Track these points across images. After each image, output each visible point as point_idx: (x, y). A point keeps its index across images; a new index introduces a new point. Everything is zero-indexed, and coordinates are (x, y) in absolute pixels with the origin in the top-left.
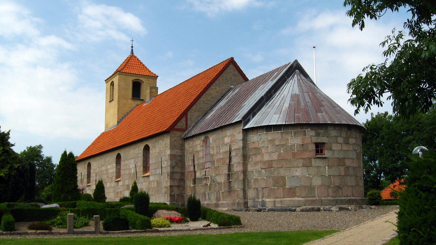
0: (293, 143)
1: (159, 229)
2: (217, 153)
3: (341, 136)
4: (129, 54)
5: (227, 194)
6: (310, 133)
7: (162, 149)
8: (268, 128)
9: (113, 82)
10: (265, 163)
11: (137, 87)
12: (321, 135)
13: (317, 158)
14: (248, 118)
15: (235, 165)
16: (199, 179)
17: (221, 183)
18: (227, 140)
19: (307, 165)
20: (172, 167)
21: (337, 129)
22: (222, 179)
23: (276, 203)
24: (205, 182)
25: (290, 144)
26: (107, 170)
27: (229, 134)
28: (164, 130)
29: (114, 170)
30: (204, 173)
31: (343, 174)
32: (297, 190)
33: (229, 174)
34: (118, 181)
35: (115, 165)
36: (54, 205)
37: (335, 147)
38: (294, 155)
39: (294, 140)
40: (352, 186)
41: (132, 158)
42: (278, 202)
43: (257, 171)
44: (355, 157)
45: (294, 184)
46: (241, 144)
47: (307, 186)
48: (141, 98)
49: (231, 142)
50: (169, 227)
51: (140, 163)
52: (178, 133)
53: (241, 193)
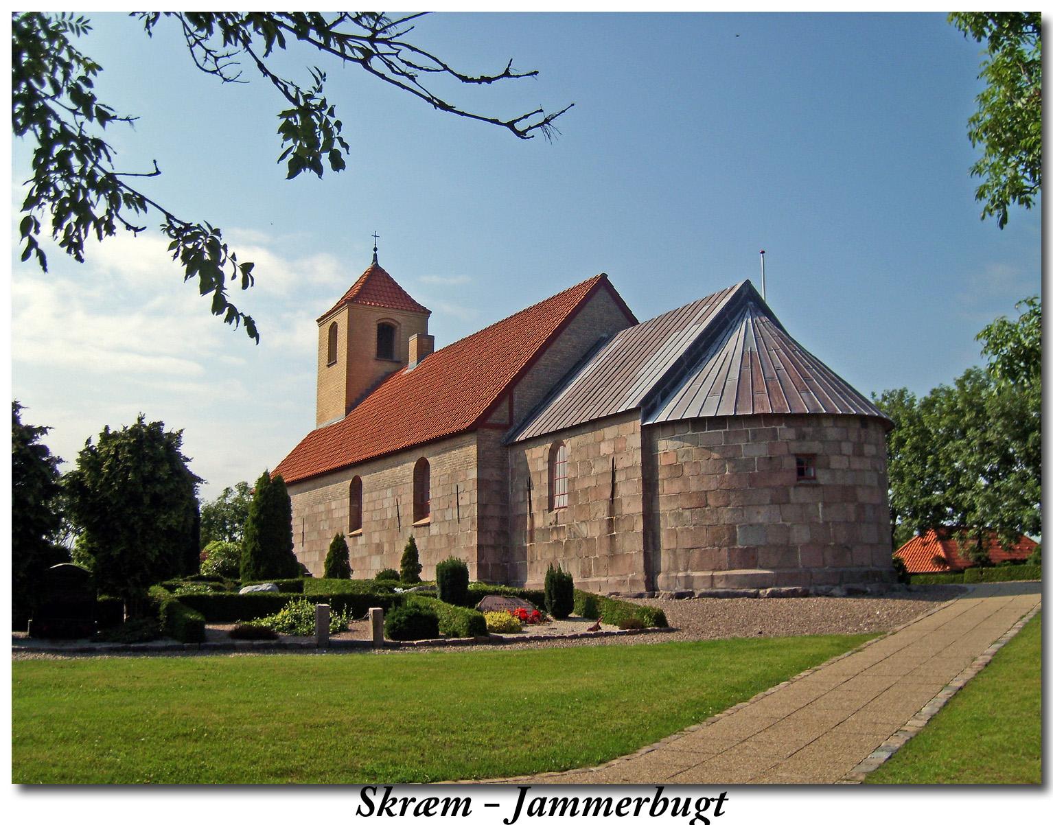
0: (752, 455)
1: (505, 636)
2: (583, 476)
3: (847, 440)
4: (367, 265)
5: (606, 561)
6: (786, 432)
7: (457, 469)
8: (698, 423)
9: (335, 323)
10: (690, 496)
11: (387, 336)
12: (808, 438)
13: (801, 485)
14: (653, 401)
15: (625, 501)
16: (540, 530)
17: (593, 539)
18: (606, 448)
19: (780, 500)
20: (482, 506)
21: (840, 424)
22: (595, 531)
23: (716, 581)
24: (554, 537)
25: (743, 457)
26: (330, 511)
27: (611, 437)
28: (465, 426)
29: (347, 511)
30: (552, 519)
31: (853, 519)
32: (760, 554)
33: (610, 521)
34: (356, 536)
35: (348, 500)
36: (265, 586)
37: (836, 462)
38: (753, 480)
39: (754, 450)
40: (872, 545)
41: (389, 488)
42: (719, 577)
43: (673, 514)
44: (875, 483)
45: (752, 541)
46: (638, 458)
47: (782, 545)
48: (396, 358)
49: (615, 452)
50: (520, 631)
51: (408, 497)
52: (493, 434)
53: (640, 561)
